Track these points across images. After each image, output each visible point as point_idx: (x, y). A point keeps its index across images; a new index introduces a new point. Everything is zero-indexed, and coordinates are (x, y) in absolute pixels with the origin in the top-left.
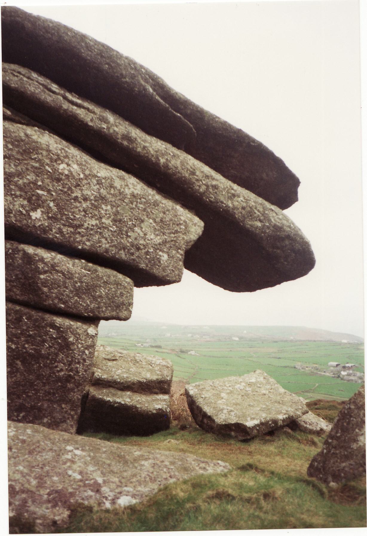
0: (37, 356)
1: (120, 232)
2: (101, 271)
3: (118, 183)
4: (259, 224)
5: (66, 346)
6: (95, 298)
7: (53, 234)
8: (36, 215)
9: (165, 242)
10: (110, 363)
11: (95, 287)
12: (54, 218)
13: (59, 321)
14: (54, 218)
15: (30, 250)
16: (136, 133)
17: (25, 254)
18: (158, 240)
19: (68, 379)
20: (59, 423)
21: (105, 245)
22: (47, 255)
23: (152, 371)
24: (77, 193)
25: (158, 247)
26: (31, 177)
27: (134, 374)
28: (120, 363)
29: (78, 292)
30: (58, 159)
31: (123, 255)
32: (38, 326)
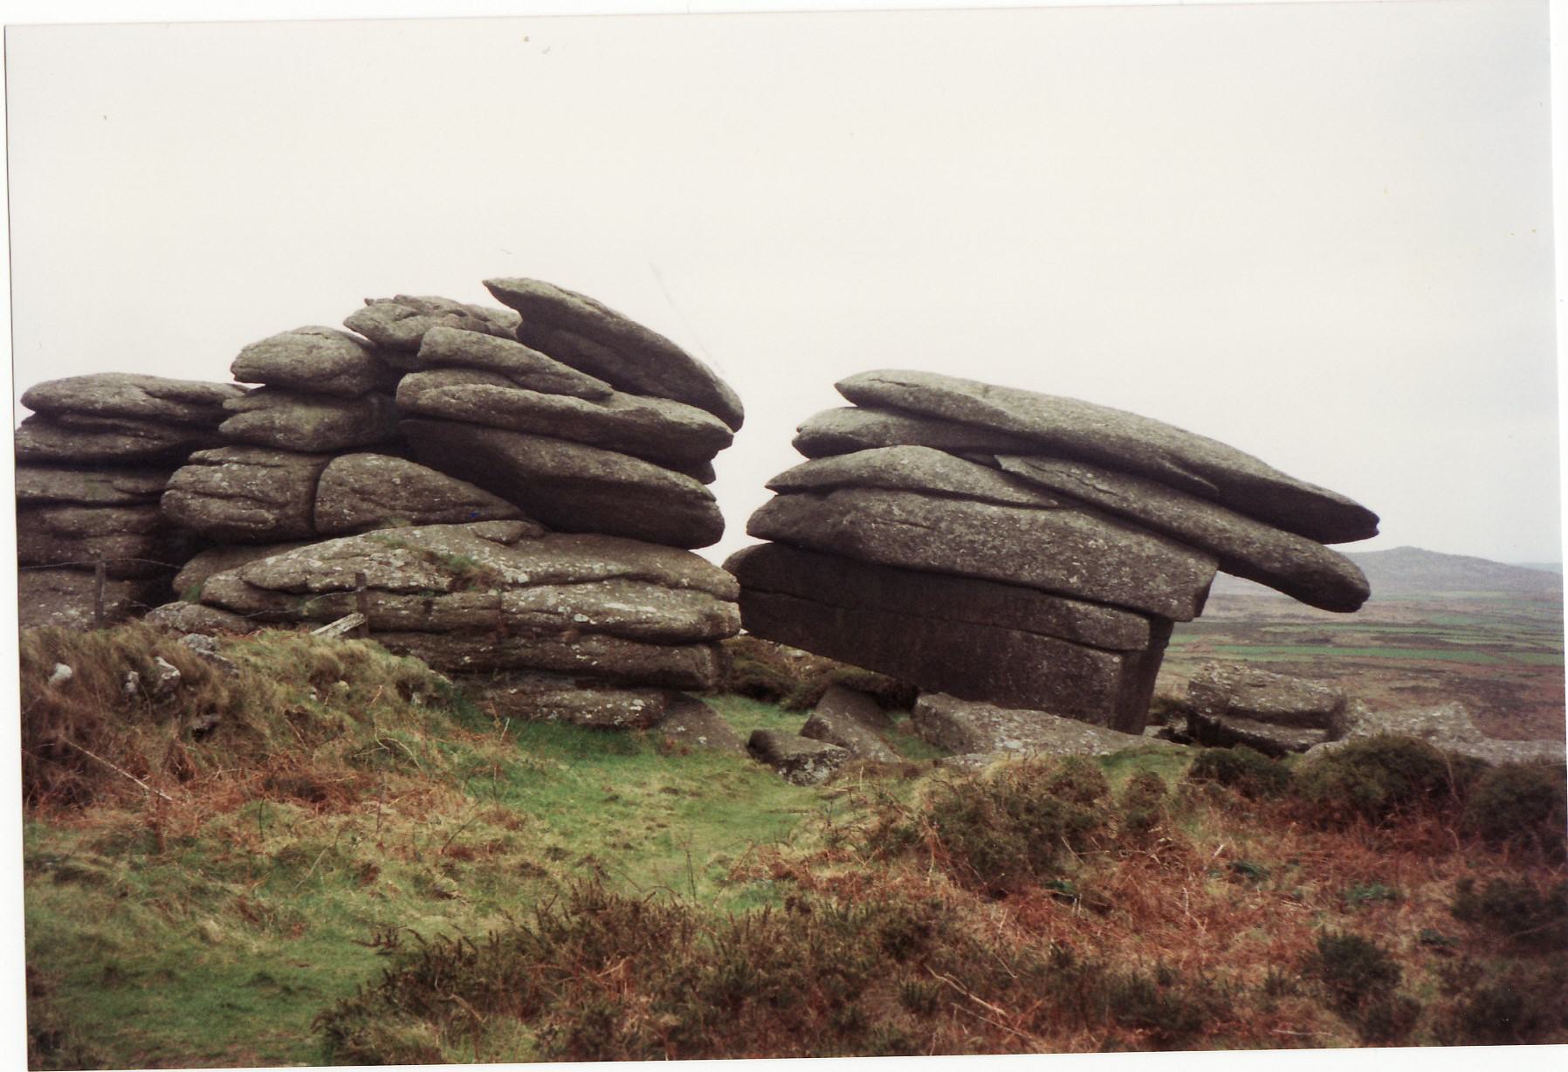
0: (1080, 677)
1: (1136, 587)
2: (1122, 615)
3: (1135, 549)
4: (1277, 565)
5: (1097, 670)
6: (1117, 637)
7: (1086, 593)
8: (1074, 580)
9: (1175, 591)
10: (1254, 690)
11: (1117, 628)
12: (1087, 581)
13: (1092, 652)
14: (1087, 581)
15: (1071, 604)
16: (672, 475)
17: (1068, 609)
18: (1169, 590)
19: (1101, 692)
20: (701, 688)
21: (1124, 597)
22: (1081, 607)
23: (1307, 700)
24: (1103, 561)
25: (1168, 596)
26: (1068, 554)
27: (1283, 704)
28: (1268, 690)
29: (1104, 632)
30: (1089, 538)
31: (1140, 604)
32: (1079, 656)
